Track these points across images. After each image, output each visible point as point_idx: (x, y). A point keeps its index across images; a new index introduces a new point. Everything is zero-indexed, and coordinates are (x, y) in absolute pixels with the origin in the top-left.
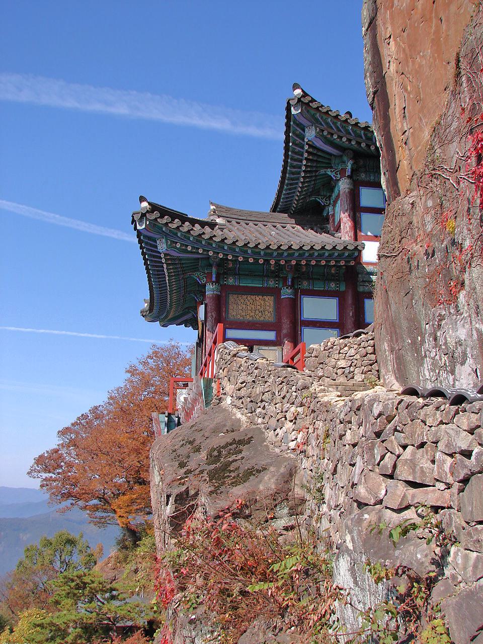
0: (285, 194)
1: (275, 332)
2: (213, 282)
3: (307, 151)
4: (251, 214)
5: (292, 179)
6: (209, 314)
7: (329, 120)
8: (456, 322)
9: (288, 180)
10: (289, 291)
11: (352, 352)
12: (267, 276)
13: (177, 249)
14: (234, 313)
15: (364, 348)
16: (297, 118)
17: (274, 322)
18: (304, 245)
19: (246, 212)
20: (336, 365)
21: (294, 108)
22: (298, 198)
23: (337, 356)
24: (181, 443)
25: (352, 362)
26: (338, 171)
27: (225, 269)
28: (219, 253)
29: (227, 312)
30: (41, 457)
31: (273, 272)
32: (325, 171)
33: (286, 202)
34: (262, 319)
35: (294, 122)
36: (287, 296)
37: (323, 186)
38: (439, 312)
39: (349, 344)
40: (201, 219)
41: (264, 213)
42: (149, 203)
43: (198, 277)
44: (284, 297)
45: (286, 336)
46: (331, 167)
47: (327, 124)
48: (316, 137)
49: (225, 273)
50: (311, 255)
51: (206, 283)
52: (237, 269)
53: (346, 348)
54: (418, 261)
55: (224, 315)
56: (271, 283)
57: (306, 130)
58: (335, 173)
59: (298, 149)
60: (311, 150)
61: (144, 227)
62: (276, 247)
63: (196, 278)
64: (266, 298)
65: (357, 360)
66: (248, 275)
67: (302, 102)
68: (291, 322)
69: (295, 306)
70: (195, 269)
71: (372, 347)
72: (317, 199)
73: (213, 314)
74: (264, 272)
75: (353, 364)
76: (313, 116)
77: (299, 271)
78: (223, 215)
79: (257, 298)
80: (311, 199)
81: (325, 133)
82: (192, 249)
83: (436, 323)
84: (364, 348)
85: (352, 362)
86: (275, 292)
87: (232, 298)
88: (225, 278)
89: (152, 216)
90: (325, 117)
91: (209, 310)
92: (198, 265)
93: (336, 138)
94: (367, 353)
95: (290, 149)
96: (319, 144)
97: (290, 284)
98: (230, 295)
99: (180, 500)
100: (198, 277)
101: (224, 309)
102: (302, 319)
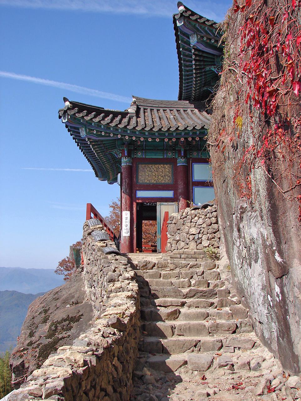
0: (185, 87)
1: (173, 191)
2: (126, 156)
3: (194, 54)
4: (162, 102)
5: (188, 76)
6: (124, 180)
7: (206, 28)
8: (250, 219)
9: (185, 76)
10: (183, 160)
11: (200, 221)
12: (167, 150)
13: (94, 134)
14: (143, 179)
15: (210, 218)
16: (182, 29)
17: (172, 184)
18: (188, 126)
19: (158, 101)
20: (189, 231)
21: (179, 21)
22: (195, 88)
23: (189, 224)
24: (147, 257)
25: (201, 230)
26: (219, 67)
27: (136, 146)
28: (126, 136)
29: (137, 178)
30: (64, 261)
31: (171, 146)
32: (210, 68)
33: (187, 92)
34: (163, 182)
35: (181, 33)
36: (181, 164)
37: (212, 79)
38: (241, 205)
39: (198, 215)
40: (115, 111)
41: (171, 101)
42: (70, 102)
43: (116, 153)
44: (179, 165)
45: (181, 194)
46: (214, 65)
47: (206, 32)
48: (197, 42)
49: (135, 149)
50: (195, 134)
51: (121, 157)
52: (144, 146)
53: (196, 218)
54: (229, 152)
55: (135, 180)
56: (170, 155)
57: (190, 37)
58: (218, 69)
59: (187, 53)
60: (197, 53)
61: (66, 120)
62: (166, 129)
63: (114, 154)
64: (166, 166)
65: (204, 228)
66: (152, 150)
67: (184, 16)
68: (184, 183)
69: (187, 171)
70: (115, 147)
71: (215, 217)
72: (208, 88)
73: (126, 180)
74: (164, 147)
75: (201, 232)
76: (194, 26)
77: (191, 144)
78: (141, 105)
79: (160, 167)
80: (204, 89)
81: (205, 39)
82: (105, 134)
83: (239, 215)
84: (210, 218)
85: (201, 230)
86: (172, 162)
87: (141, 167)
88: (135, 153)
89: (72, 112)
90: (203, 26)
91: (123, 177)
92: (116, 144)
93: (213, 42)
94: (211, 223)
95: (182, 53)
96: (201, 47)
97: (183, 155)
98: (140, 165)
99: (17, 371)
100: (116, 153)
101: (135, 176)
102: (193, 180)
